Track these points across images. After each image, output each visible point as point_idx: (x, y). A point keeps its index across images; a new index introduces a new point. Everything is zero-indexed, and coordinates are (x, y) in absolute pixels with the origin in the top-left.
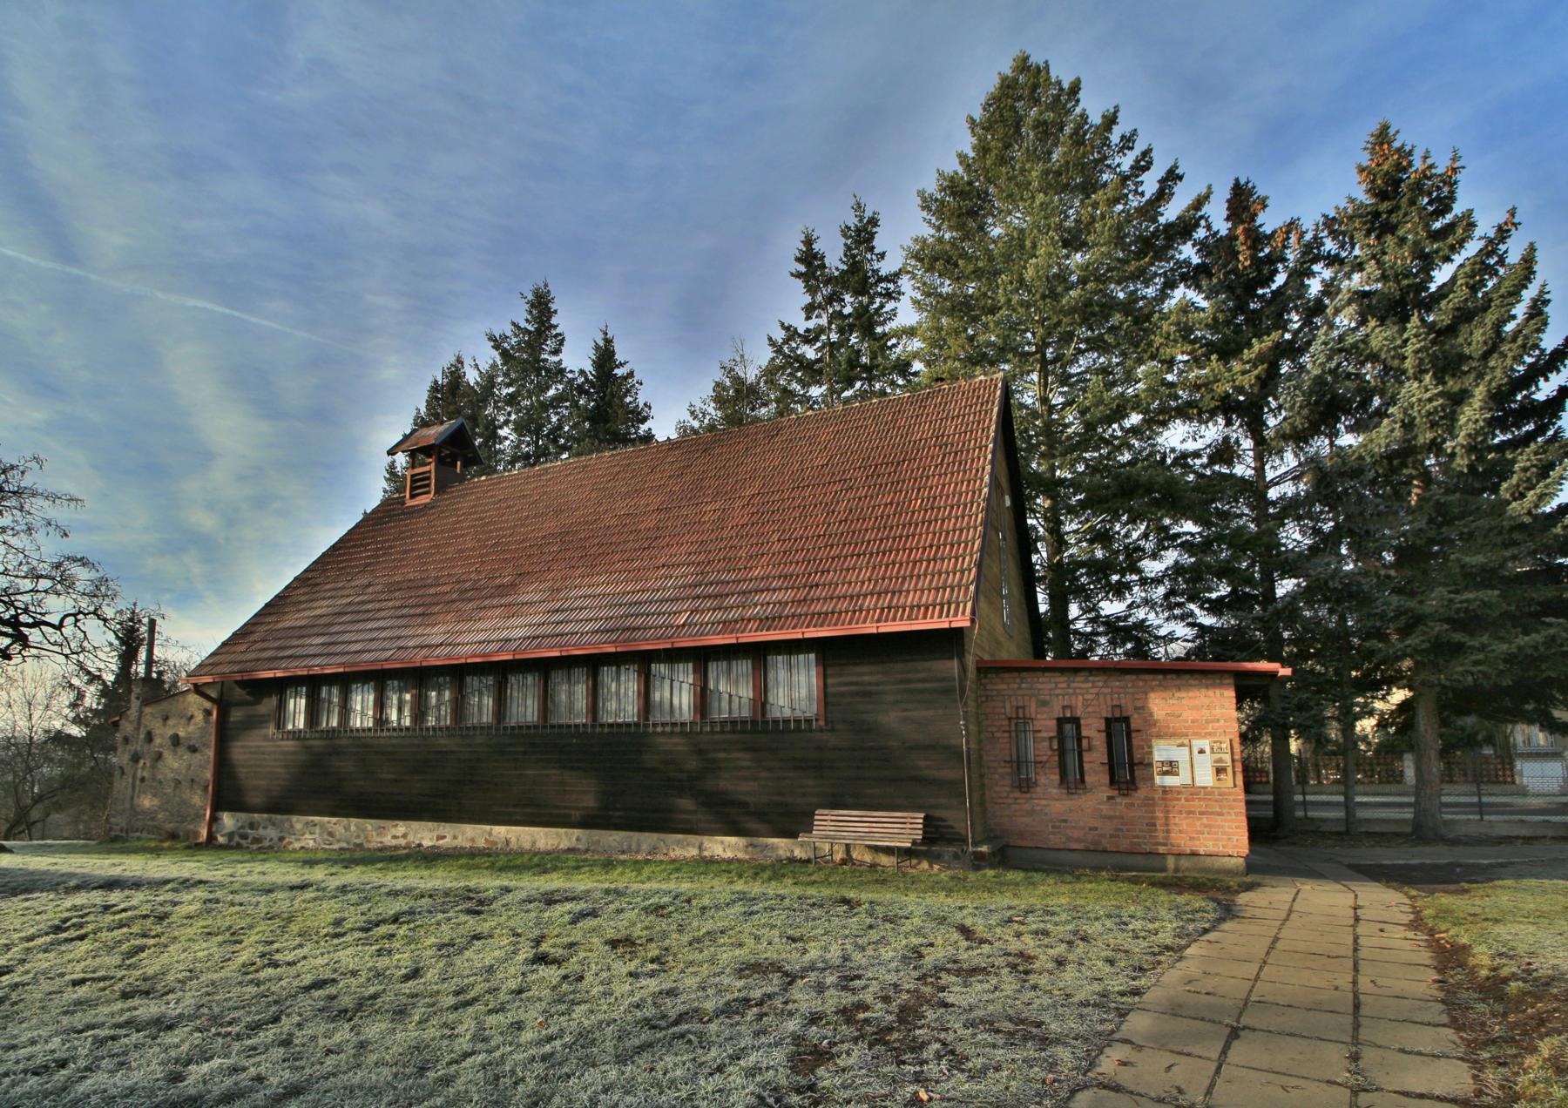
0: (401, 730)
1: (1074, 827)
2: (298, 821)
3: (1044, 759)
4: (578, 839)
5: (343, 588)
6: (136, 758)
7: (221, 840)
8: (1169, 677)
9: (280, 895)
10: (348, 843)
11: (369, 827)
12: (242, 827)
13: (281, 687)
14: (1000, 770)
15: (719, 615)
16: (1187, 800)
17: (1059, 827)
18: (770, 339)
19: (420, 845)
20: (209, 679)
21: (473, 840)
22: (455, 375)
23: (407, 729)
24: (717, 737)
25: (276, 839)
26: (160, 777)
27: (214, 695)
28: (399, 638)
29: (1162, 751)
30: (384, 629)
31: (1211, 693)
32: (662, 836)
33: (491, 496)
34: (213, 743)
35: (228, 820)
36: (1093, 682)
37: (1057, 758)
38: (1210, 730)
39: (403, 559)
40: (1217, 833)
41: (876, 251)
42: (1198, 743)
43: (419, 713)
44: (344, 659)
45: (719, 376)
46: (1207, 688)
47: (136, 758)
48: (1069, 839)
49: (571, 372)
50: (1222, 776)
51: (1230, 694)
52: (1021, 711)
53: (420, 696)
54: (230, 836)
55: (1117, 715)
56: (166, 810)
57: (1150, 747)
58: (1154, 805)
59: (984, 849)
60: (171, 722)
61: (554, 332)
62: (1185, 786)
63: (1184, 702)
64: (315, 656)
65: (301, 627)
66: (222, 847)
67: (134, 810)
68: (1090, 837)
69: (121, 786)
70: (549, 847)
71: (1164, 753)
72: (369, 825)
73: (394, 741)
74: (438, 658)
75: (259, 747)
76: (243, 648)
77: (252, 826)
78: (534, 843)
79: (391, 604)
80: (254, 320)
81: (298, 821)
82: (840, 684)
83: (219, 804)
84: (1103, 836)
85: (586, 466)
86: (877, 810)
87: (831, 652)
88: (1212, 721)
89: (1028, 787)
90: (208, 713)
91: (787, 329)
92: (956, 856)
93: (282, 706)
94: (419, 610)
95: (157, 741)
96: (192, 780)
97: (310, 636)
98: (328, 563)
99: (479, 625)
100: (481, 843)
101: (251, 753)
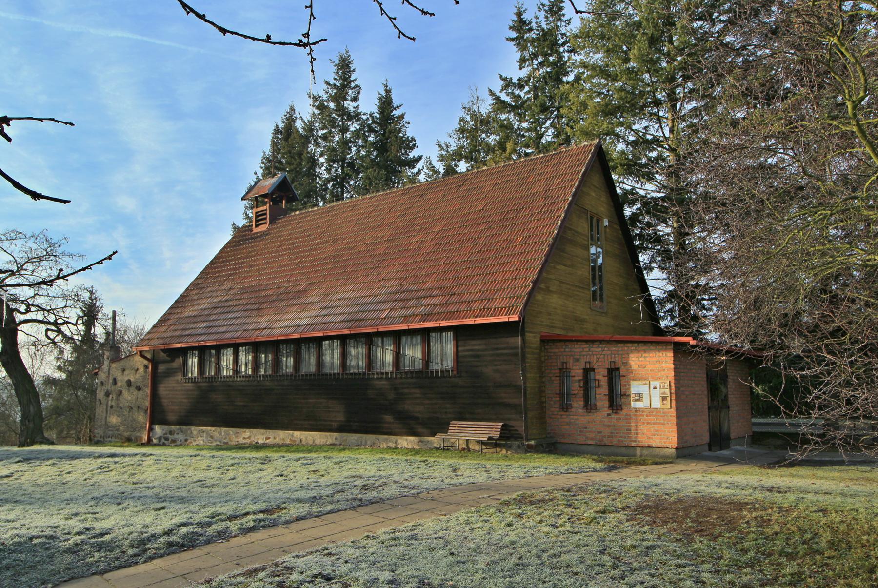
0: (246, 377)
1: (590, 432)
2: (195, 430)
3: (576, 392)
4: (336, 439)
5: (217, 291)
6: (107, 394)
7: (155, 441)
8: (640, 345)
9: (186, 458)
10: (221, 442)
11: (231, 433)
12: (166, 434)
13: (183, 352)
14: (554, 399)
15: (403, 312)
16: (647, 416)
17: (582, 432)
18: (490, 91)
19: (257, 443)
20: (147, 348)
21: (284, 439)
22: (290, 120)
23: (250, 376)
24: (404, 380)
25: (183, 440)
26: (121, 405)
27: (149, 356)
28: (245, 324)
29: (635, 388)
30: (238, 318)
31: (661, 354)
32: (377, 436)
33: (300, 227)
34: (150, 385)
35: (158, 430)
36: (602, 348)
37: (582, 392)
38: (660, 376)
39: (249, 272)
40: (661, 435)
41: (564, 19)
42: (655, 383)
43: (256, 366)
44: (216, 337)
45: (462, 113)
46: (659, 351)
47: (107, 394)
48: (587, 438)
49: (365, 114)
50: (665, 402)
51: (670, 354)
52: (613, 364)
53: (256, 357)
54: (160, 438)
55: (613, 367)
56: (124, 425)
57: (629, 385)
58: (630, 419)
59: (532, 442)
60: (126, 372)
61: (353, 85)
62: (646, 408)
63: (647, 359)
64: (202, 334)
65: (195, 316)
66: (155, 445)
67: (107, 426)
68: (598, 437)
69: (100, 411)
70: (322, 443)
71: (636, 389)
72: (231, 431)
73: (243, 383)
74: (263, 336)
75: (173, 387)
76: (164, 329)
77: (171, 433)
78: (314, 441)
79: (241, 302)
80: (159, 42)
81: (195, 430)
82: (464, 351)
83: (153, 422)
84: (604, 436)
85: (355, 206)
86: (481, 421)
87: (461, 333)
88: (661, 371)
89: (567, 408)
90: (146, 367)
91: (505, 79)
92: (519, 447)
93: (185, 363)
94: (256, 307)
95: (119, 384)
96: (139, 407)
97: (199, 322)
98: (209, 273)
99: (286, 317)
100: (288, 442)
101: (169, 391)
